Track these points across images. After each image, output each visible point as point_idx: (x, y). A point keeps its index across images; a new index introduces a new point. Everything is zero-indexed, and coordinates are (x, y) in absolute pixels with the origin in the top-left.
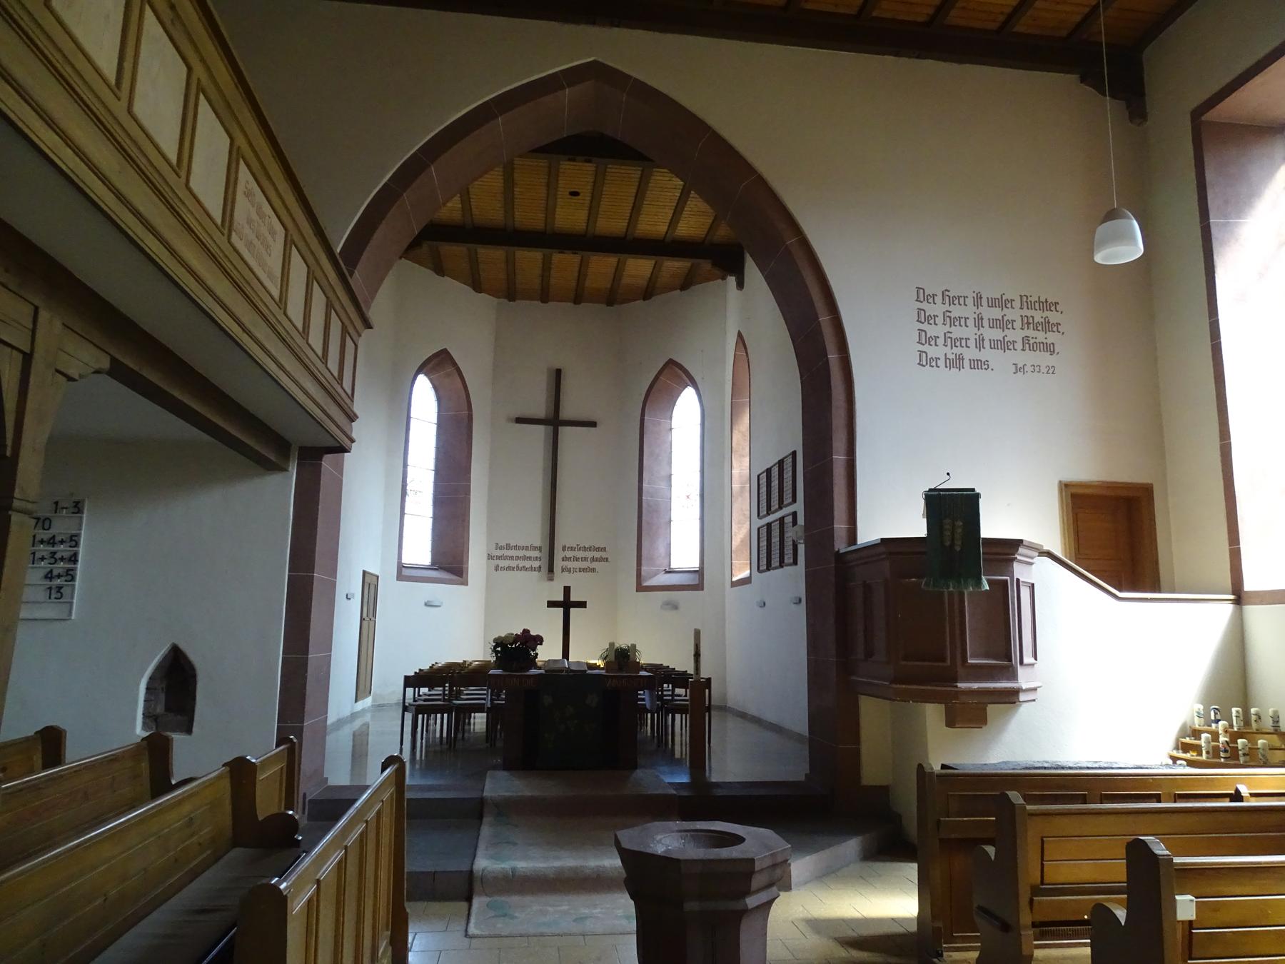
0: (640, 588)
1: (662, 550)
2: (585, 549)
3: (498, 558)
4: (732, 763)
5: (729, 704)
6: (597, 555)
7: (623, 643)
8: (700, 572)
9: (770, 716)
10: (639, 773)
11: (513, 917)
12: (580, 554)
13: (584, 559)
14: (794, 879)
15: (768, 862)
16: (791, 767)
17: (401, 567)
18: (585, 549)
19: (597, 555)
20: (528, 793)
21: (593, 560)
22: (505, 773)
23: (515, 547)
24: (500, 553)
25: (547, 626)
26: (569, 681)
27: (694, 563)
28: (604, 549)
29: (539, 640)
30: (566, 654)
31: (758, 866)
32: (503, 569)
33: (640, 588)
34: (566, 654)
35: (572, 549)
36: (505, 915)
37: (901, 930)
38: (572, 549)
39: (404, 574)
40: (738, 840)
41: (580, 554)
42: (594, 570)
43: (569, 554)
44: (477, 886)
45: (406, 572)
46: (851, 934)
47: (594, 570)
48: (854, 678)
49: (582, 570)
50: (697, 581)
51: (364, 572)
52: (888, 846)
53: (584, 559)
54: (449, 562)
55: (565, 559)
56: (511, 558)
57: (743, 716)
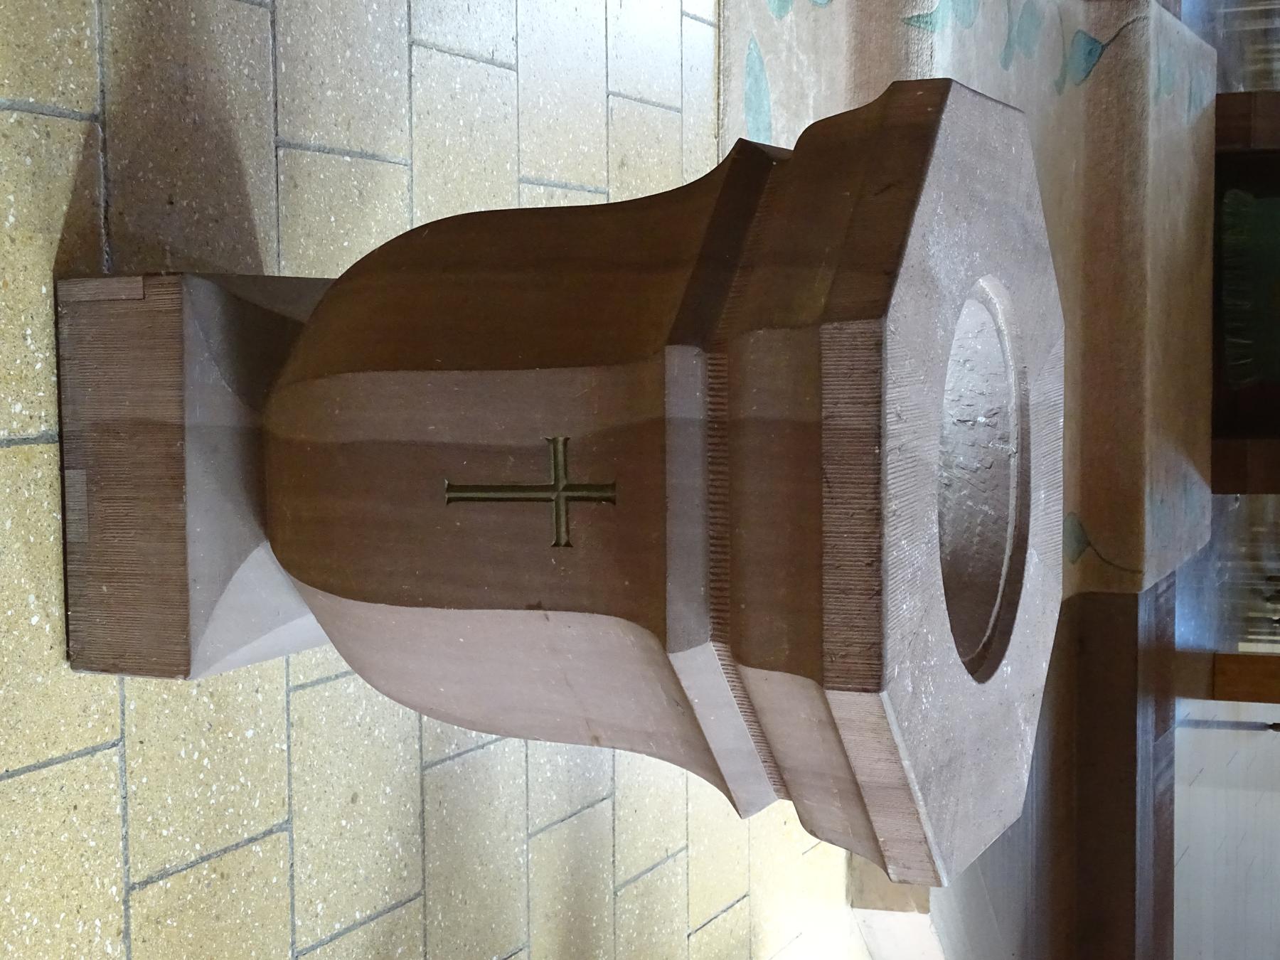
10: (1202, 495)
15: (870, 766)
20: (1153, 134)
22: (1208, 97)
31: (847, 703)
40: (983, 658)
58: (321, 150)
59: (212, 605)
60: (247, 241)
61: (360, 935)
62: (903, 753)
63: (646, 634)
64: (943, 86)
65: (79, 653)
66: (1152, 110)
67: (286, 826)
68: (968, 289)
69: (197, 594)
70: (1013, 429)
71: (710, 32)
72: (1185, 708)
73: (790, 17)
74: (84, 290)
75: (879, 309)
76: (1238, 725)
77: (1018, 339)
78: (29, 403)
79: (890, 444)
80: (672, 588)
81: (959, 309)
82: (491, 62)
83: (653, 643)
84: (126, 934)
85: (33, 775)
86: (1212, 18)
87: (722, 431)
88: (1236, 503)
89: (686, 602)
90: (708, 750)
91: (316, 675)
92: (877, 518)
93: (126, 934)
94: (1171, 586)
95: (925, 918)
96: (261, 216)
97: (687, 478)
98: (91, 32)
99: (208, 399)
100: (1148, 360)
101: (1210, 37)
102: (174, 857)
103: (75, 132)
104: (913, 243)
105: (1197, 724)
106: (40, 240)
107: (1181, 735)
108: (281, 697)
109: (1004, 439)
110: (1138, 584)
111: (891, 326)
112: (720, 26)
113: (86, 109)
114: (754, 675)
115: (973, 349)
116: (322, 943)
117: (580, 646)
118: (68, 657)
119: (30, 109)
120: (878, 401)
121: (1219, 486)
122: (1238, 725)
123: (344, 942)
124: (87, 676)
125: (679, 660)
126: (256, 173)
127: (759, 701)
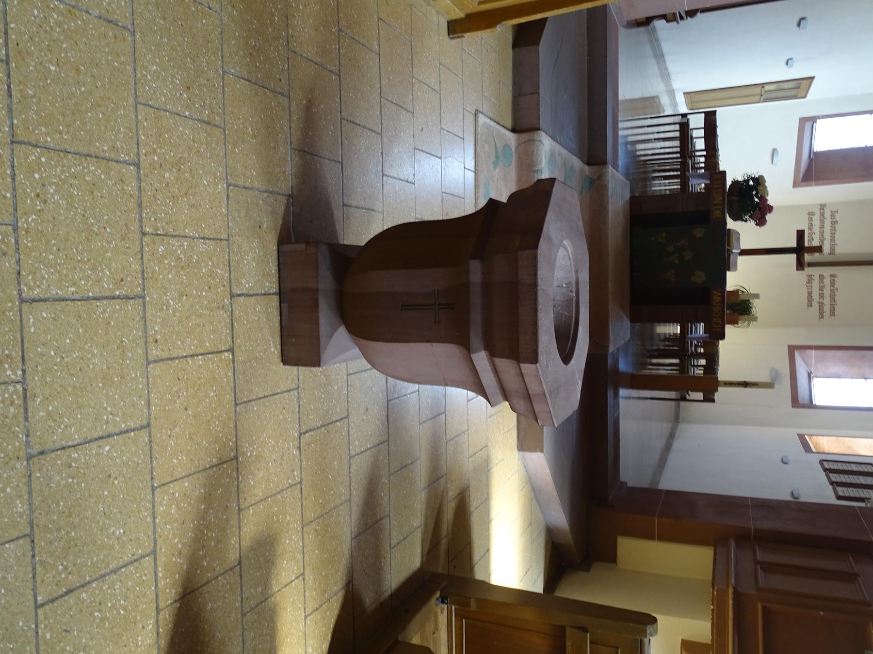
0: (792, 349)
1: (834, 369)
2: (833, 297)
3: (822, 215)
4: (636, 415)
5: (682, 426)
6: (827, 308)
7: (757, 306)
8: (810, 405)
9: (673, 459)
10: (627, 323)
11: (495, 164)
12: (827, 292)
13: (822, 296)
14: (528, 455)
15: (533, 388)
16: (632, 470)
17: (813, 120)
18: (833, 297)
19: (827, 308)
20: (611, 208)
21: (821, 305)
22: (627, 196)
23: (833, 229)
24: (828, 214)
25: (778, 231)
26: (720, 253)
27: (818, 401)
28: (833, 313)
29: (761, 222)
30: (745, 252)
31: (526, 368)
32: (811, 219)
33: (792, 349)
34: (745, 252)
35: (833, 284)
36: (497, 157)
37: (477, 555)
38: (833, 284)
39: (807, 123)
40: (566, 358)
41: (827, 292)
42: (810, 305)
43: (827, 281)
44: (525, 137)
45: (808, 125)
46: (474, 504)
47: (810, 305)
48: (733, 544)
49: (810, 294)
50: (800, 402)
51: (812, 78)
52: (562, 558)
53: (822, 296)
54: (817, 168)
55: (821, 278)
56: (822, 226)
57: (672, 436)
58: (356, 207)
59: (326, 345)
60: (335, 235)
61: (369, 452)
62: (543, 383)
63: (462, 348)
64: (552, 181)
65: (286, 360)
66: (610, 200)
67: (347, 417)
68: (561, 244)
69: (323, 341)
70: (574, 289)
71: (473, 174)
72: (622, 392)
73: (497, 170)
74: (288, 248)
75: (536, 246)
76: (639, 398)
77: (575, 260)
78: (270, 282)
79: (539, 288)
80: (472, 335)
81: (558, 249)
82: (407, 181)
83: (465, 352)
84: (299, 448)
85: (272, 397)
86: (628, 173)
87: (487, 285)
88: (638, 326)
89: (476, 339)
90: (482, 386)
91: (355, 371)
92: (535, 310)
93: (299, 448)
94: (618, 352)
95: (542, 455)
96: (339, 227)
97: (476, 300)
98: (288, 170)
99: (326, 281)
100: (610, 285)
101: (628, 179)
102: (313, 426)
103: (284, 199)
104: (545, 226)
105: (626, 398)
106: (274, 233)
107: (622, 402)
108: (345, 377)
109: (571, 291)
110: (608, 351)
111: (539, 252)
112: (476, 172)
113: (287, 193)
114: (497, 361)
115: (562, 262)
116: (358, 454)
117: (445, 353)
118: (282, 361)
119: (270, 192)
120: (535, 275)
121: (633, 320)
122: (639, 398)
123: (365, 454)
124: (287, 367)
125: (473, 356)
126: (337, 214)
127: (499, 369)
